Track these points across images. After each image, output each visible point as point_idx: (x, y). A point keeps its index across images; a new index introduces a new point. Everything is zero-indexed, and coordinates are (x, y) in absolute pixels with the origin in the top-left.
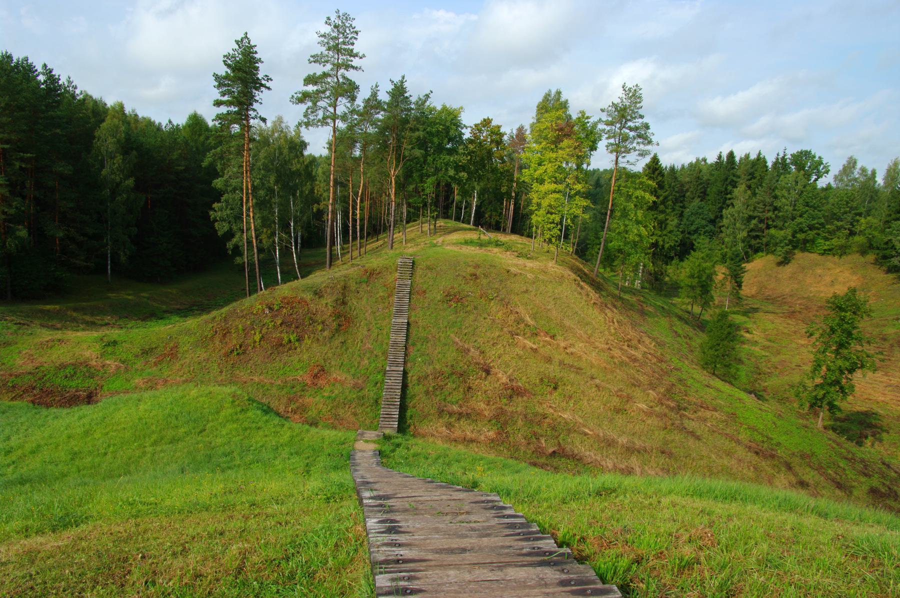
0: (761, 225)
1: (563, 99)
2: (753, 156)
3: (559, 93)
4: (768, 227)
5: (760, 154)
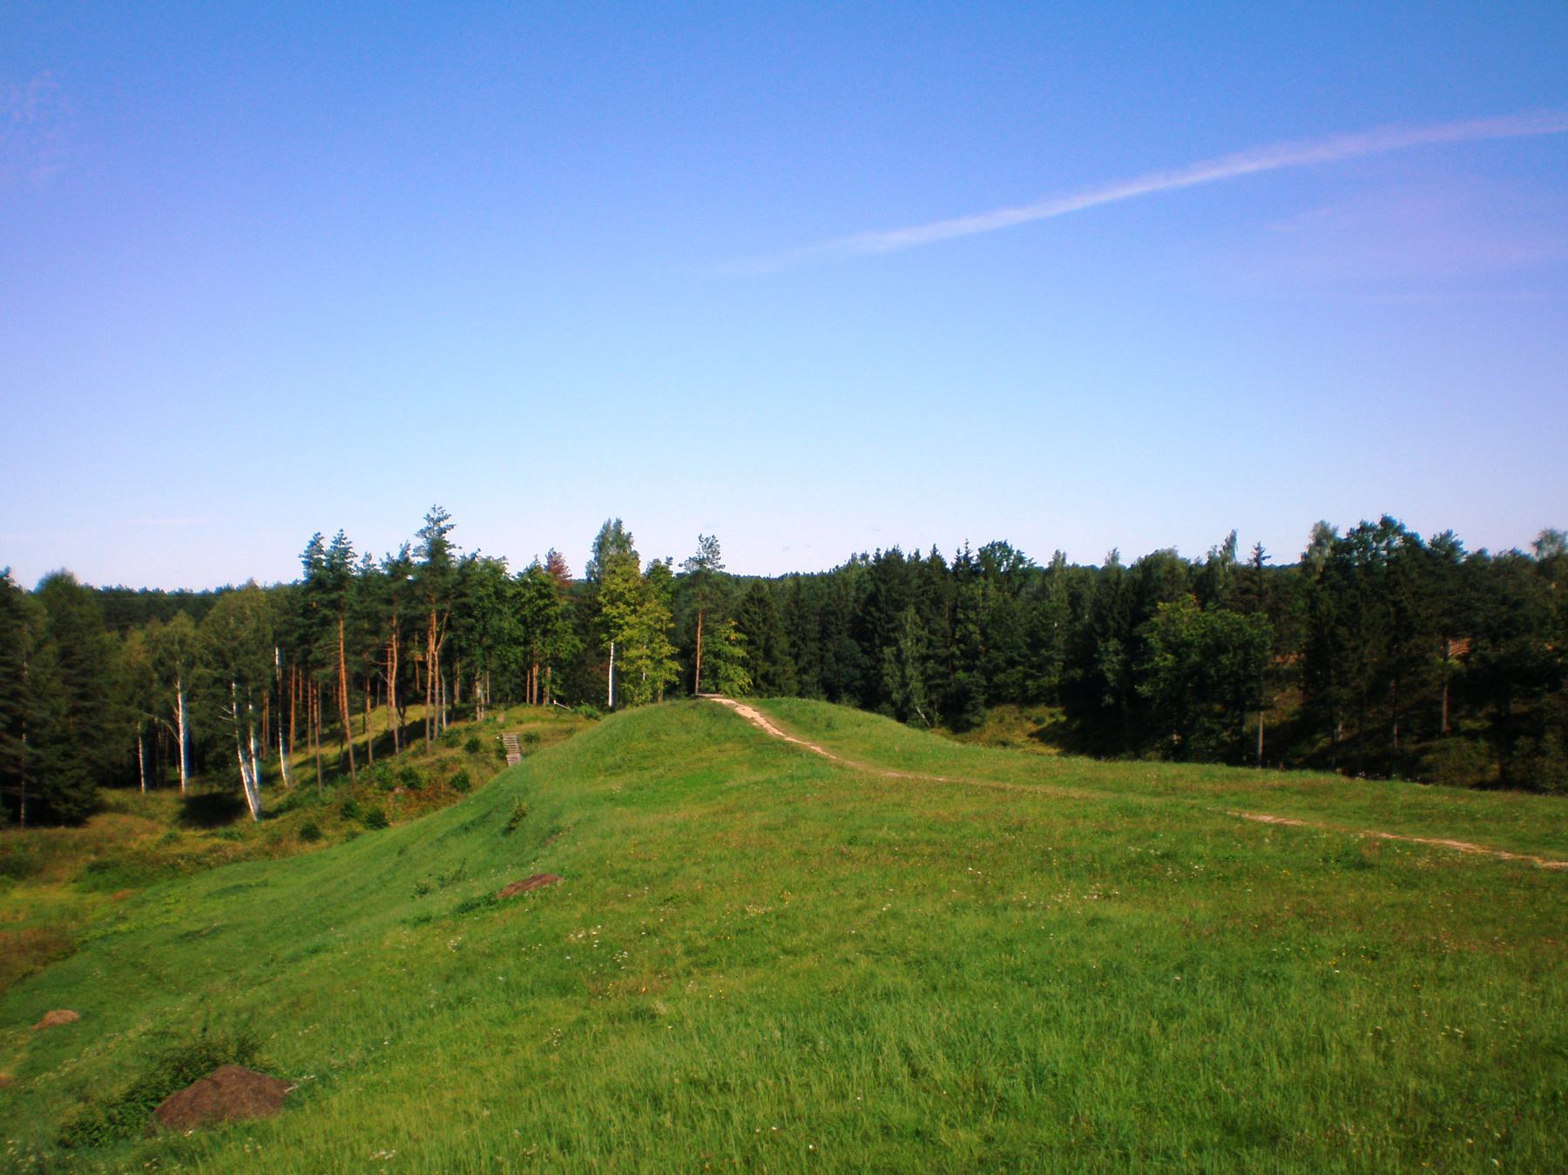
0: (942, 669)
1: (625, 531)
2: (925, 555)
3: (619, 523)
4: (955, 669)
5: (935, 550)
